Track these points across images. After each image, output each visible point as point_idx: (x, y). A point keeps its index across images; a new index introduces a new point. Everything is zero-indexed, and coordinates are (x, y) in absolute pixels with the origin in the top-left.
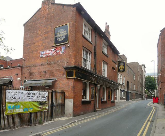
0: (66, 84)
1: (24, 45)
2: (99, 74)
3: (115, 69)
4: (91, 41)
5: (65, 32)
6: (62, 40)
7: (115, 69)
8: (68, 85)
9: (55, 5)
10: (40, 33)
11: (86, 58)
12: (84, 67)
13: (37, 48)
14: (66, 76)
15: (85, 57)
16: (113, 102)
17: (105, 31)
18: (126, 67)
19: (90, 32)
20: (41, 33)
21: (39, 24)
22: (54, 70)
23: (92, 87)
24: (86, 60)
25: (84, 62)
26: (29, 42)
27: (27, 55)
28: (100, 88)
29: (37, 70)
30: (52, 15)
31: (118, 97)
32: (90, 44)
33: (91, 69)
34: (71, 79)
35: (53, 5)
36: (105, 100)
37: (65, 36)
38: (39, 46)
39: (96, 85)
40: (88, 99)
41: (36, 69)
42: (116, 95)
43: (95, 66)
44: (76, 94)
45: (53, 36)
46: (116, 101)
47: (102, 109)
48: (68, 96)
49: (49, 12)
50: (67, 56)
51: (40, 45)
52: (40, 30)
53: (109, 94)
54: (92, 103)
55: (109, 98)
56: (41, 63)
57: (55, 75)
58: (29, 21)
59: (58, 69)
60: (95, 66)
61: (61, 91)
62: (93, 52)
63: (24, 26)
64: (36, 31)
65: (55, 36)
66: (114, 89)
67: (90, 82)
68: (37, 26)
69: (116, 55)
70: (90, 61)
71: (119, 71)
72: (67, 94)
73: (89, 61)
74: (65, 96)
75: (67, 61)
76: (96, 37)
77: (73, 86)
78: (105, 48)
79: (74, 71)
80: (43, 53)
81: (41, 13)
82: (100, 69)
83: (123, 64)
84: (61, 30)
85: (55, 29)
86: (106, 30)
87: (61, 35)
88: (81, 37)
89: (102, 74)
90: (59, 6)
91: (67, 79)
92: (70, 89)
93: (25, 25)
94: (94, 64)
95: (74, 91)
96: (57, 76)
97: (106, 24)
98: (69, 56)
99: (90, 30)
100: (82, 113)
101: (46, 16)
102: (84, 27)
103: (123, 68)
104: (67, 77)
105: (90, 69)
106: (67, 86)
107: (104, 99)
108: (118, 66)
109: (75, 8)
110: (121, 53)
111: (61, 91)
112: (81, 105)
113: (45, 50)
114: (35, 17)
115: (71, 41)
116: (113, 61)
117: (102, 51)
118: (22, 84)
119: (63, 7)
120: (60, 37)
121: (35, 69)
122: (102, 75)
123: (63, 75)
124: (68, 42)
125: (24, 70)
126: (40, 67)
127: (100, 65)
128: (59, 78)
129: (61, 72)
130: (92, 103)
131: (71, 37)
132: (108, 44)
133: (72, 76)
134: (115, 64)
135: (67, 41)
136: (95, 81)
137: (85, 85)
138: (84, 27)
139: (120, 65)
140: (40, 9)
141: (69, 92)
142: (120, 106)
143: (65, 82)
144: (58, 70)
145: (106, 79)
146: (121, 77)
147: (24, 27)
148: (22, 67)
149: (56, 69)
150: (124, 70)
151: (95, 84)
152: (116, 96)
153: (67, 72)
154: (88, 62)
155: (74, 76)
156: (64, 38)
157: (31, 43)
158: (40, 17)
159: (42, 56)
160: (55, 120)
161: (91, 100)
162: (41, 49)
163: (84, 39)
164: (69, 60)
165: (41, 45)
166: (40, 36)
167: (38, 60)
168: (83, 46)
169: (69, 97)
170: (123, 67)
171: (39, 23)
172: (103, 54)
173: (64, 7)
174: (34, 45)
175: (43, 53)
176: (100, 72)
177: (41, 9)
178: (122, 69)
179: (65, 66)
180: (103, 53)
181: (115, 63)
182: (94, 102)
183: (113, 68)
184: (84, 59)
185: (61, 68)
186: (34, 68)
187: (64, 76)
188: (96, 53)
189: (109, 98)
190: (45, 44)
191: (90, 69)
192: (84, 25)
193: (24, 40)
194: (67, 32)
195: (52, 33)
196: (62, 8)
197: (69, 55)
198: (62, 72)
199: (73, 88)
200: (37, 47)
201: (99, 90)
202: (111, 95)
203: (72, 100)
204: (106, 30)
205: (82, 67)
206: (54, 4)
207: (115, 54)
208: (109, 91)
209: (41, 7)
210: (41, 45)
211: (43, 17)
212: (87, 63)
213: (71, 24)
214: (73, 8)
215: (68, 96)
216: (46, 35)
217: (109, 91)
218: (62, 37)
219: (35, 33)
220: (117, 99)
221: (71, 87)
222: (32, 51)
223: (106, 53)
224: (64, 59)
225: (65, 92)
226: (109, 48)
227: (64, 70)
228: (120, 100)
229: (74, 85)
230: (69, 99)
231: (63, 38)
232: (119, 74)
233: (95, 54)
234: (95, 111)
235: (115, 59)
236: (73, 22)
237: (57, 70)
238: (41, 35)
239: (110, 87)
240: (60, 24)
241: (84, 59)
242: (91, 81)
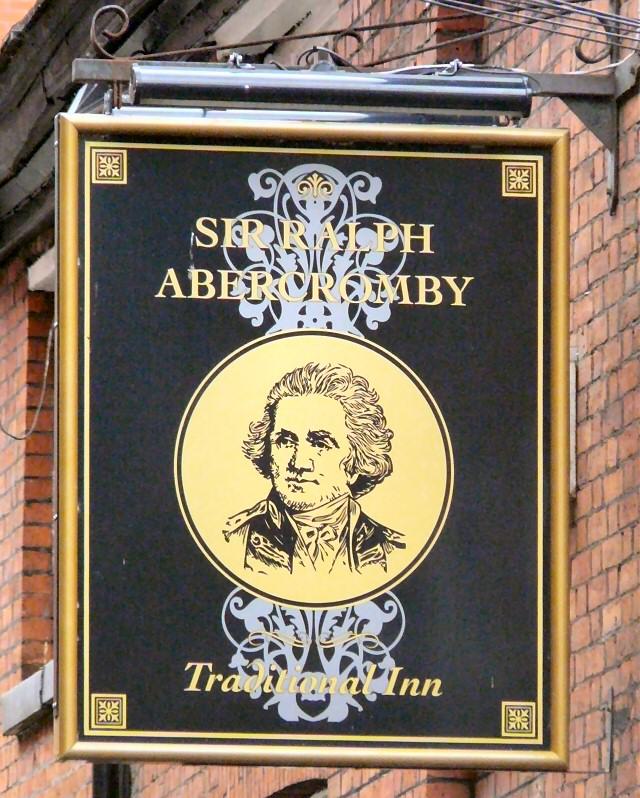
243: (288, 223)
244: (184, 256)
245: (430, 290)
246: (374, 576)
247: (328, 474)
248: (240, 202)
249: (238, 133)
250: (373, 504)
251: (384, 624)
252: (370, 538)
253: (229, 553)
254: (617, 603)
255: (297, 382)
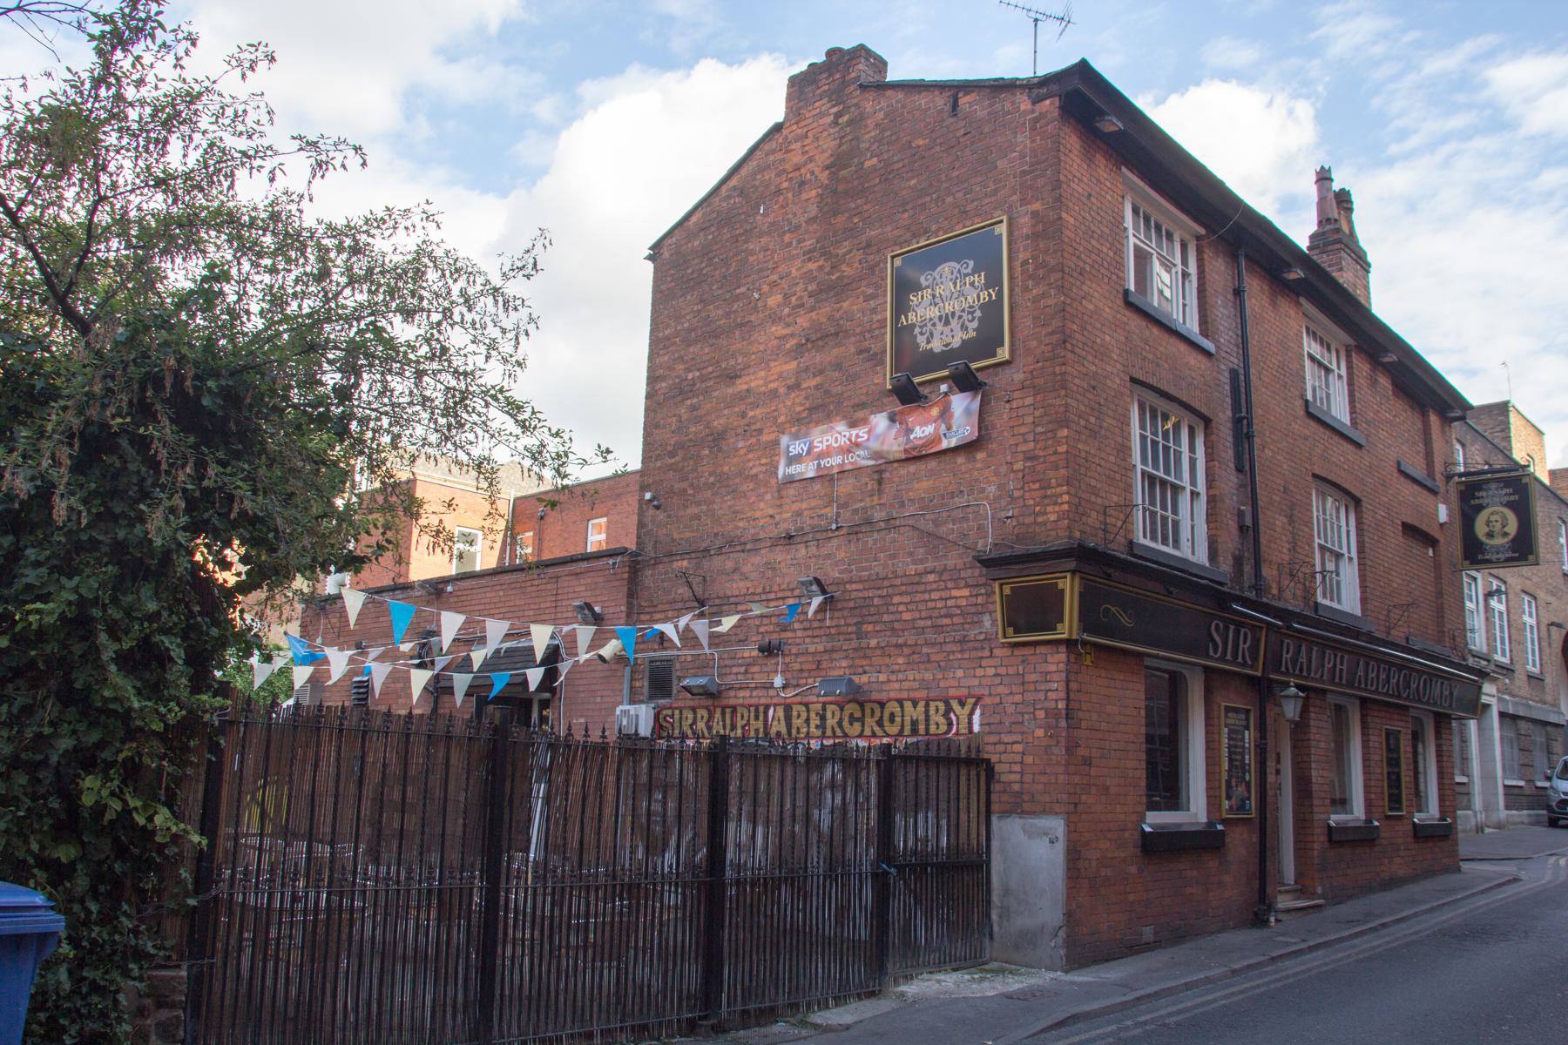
0: (1002, 690)
1: (648, 396)
2: (1288, 594)
3: (1432, 542)
4: (1196, 329)
5: (980, 279)
6: (956, 343)
7: (1432, 542)
8: (1018, 698)
9: (889, 93)
10: (779, 298)
11: (1167, 472)
12: (1148, 542)
13: (751, 414)
14: (994, 621)
15: (1156, 466)
16: (1440, 835)
17: (1312, 237)
18: (1542, 511)
19: (1185, 262)
20: (786, 297)
21: (769, 233)
22: (898, 582)
23: (1228, 709)
24: (1163, 483)
25: (1152, 502)
26: (688, 370)
27: (672, 467)
28: (1305, 710)
29: (753, 576)
30: (868, 164)
31: (1488, 777)
32: (1194, 359)
33: (1213, 554)
34: (1041, 650)
35: (871, 95)
36: (1358, 811)
37: (978, 314)
38: (774, 394)
39: (1263, 690)
40: (1196, 810)
41: (747, 568)
42: (1465, 760)
43: (1250, 531)
44: (1093, 771)
45: (876, 317)
46: (1466, 819)
47: (1338, 897)
48: (1016, 787)
49: (844, 147)
50: (1004, 469)
51: (775, 391)
52: (775, 277)
53: (1393, 762)
54: (1240, 842)
55: (1395, 800)
56: (784, 526)
57: (906, 616)
58: (694, 219)
59: (930, 565)
60: (1250, 531)
61: (963, 749)
62: (1223, 417)
63: (650, 258)
64: (743, 289)
65: (898, 319)
66: (1436, 714)
67: (1207, 669)
68: (752, 253)
69: (1433, 419)
70: (1201, 487)
71: (1474, 553)
72: (1007, 773)
73: (1194, 495)
74: (996, 787)
75: (1003, 502)
76: (1238, 292)
77: (1061, 705)
78: (1328, 370)
79: (1069, 587)
80: (797, 448)
81: (779, 156)
82: (1293, 550)
83: (1503, 494)
84: (946, 268)
85: (898, 262)
86: (1329, 227)
87: (948, 309)
88: (1110, 309)
89: (1319, 592)
90: (922, 100)
91: (1006, 652)
92: (1040, 733)
93: (657, 247)
94: (1241, 514)
95: (1071, 748)
96: (921, 623)
97: (1324, 177)
98: (1019, 466)
99: (1184, 247)
100: (1148, 933)
101: (824, 176)
102: (1131, 231)
103: (1512, 527)
104: (1010, 630)
105: (1201, 557)
106: (1010, 709)
107: (1342, 803)
108: (1458, 516)
109: (1050, 106)
110: (1476, 394)
111: (963, 749)
112: (1133, 869)
113: (817, 423)
114: (735, 188)
115: (1033, 344)
116: (1410, 471)
117: (1303, 396)
118: (631, 688)
119: (955, 106)
120: (940, 327)
121: (735, 570)
122: (1320, 599)
123: (972, 615)
124: (1004, 353)
125: (648, 577)
126: (779, 556)
127: (1291, 521)
128: (940, 639)
129: (955, 593)
130: (1240, 842)
131: (1029, 322)
132: (1350, 341)
133: (1051, 628)
134: (1431, 497)
135: (999, 351)
136: (1255, 658)
137: (1175, 687)
138: (1131, 231)
139: (1480, 508)
140: (777, 128)
141: (1029, 760)
142: (1509, 869)
143: (991, 671)
144: (931, 577)
145: (1357, 634)
146: (1494, 603)
147: (650, 266)
148: (637, 555)
149: (912, 569)
150: (1523, 549)
151: (1251, 678)
152: (1465, 773)
153: (1007, 590)
154: (1184, 500)
155: (1064, 631)
156: (975, 324)
157: (703, 379)
158: (773, 188)
159: (793, 470)
160: (911, 989)
161: (1224, 821)
162: (782, 419)
163: (1135, 322)
164: (1017, 494)
165: (782, 390)
166: (776, 319)
167: (760, 498)
168: (1133, 380)
169: (1032, 801)
170: (1512, 518)
171: (765, 228)
172: (1312, 423)
173: (964, 100)
174: (730, 391)
175: (797, 448)
176: (1292, 575)
177: (785, 132)
178: (1499, 541)
179: (986, 544)
180: (1310, 415)
181: (1434, 492)
182: (1255, 838)
183: (1410, 530)
184: (1151, 479)
185: (950, 563)
186: (729, 565)
187: (980, 622)
188: (1250, 425)
189: (1395, 800)
190: (818, 380)
191: (1201, 557)
192: (1135, 211)
193: (1160, 810)
194: (993, 281)
195: (874, 297)
196: (948, 108)
197: (1021, 456)
198: (966, 592)
199: (1063, 723)
200: (755, 406)
201: (1300, 728)
202: (1416, 762)
203: (1057, 825)
204: (1329, 227)
205: (1131, 544)
206: (883, 87)
207: (1424, 415)
208: (1388, 733)
209: (780, 118)
210: (782, 390)
211: (802, 184)
212: (1175, 512)
213: (1025, 221)
214: (1034, 103)
215: (1019, 794)
216: (822, 314)
217: (1388, 733)
218: (954, 323)
219: (737, 298)
220: (1478, 802)
221: (1041, 714)
222: (717, 438)
223: (1340, 411)
224: (983, 490)
225: (994, 759)
226: (1363, 367)
227: (982, 580)
228: (1508, 807)
229: (1068, 699)
230: (1033, 813)
231: (964, 328)
232: (1476, 583)
233: (1243, 431)
234: (1258, 913)
235: (1429, 455)
236: (1037, 206)
237: (920, 575)
238: (787, 311)
239: (1399, 697)
240: (934, 227)
241: (1151, 479)
242: (1222, 659)
243: (173, 692)
244: (1474, 498)
245: (1512, 498)
246: (1506, 540)
247: (1498, 526)
248: (1481, 489)
249: (1349, 759)
250: (1506, 529)
251: (1183, 94)
252: (1505, 534)
253: (1484, 539)
254: (774, 60)
255: (1492, 514)
